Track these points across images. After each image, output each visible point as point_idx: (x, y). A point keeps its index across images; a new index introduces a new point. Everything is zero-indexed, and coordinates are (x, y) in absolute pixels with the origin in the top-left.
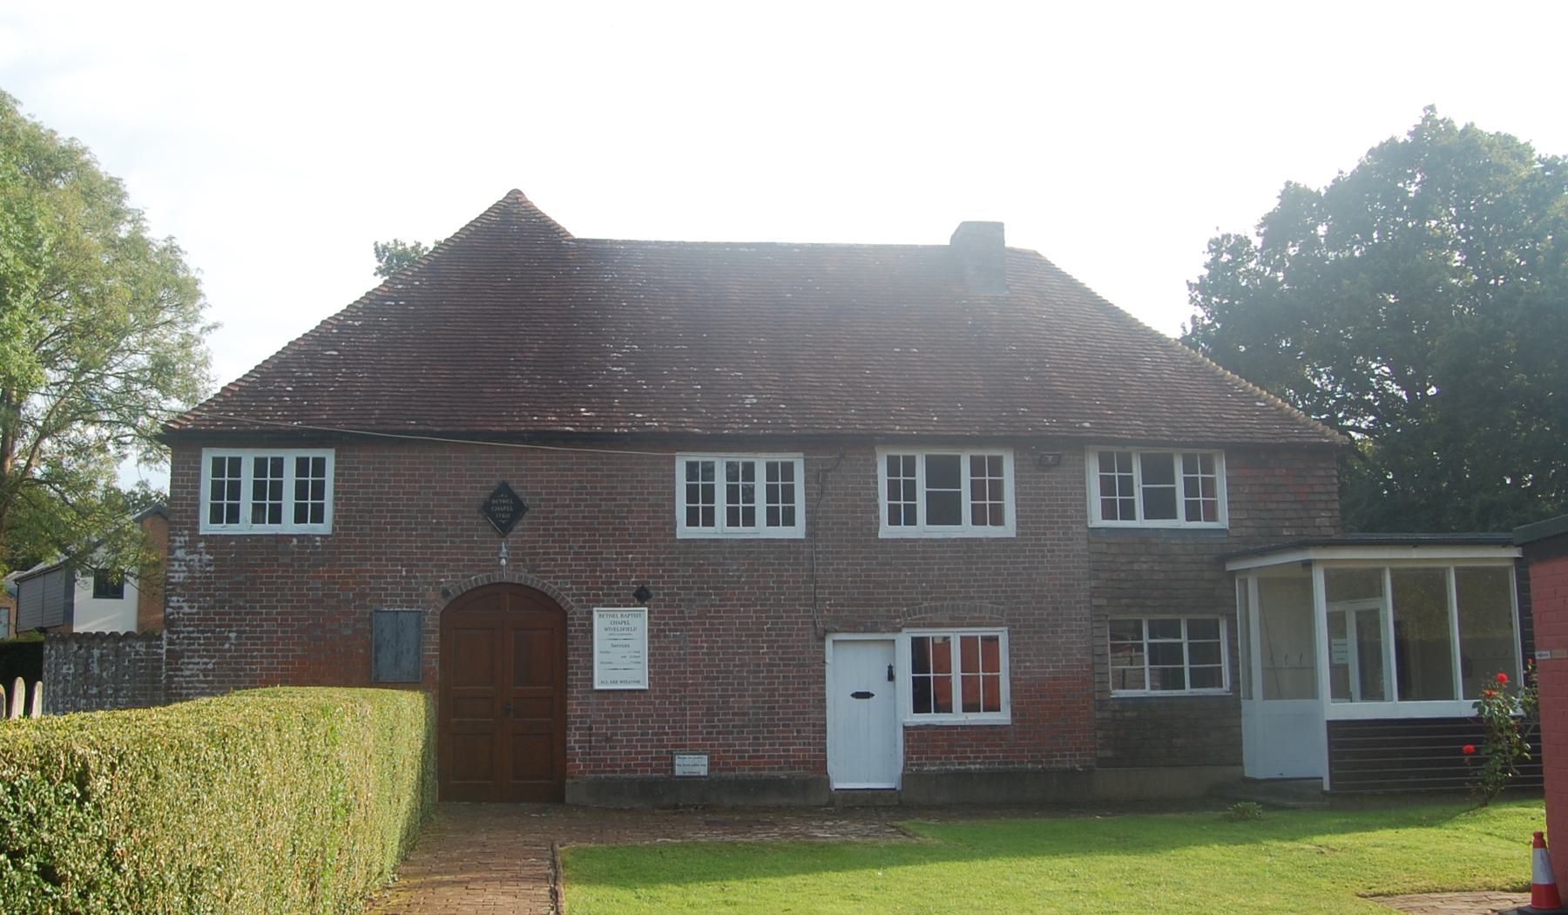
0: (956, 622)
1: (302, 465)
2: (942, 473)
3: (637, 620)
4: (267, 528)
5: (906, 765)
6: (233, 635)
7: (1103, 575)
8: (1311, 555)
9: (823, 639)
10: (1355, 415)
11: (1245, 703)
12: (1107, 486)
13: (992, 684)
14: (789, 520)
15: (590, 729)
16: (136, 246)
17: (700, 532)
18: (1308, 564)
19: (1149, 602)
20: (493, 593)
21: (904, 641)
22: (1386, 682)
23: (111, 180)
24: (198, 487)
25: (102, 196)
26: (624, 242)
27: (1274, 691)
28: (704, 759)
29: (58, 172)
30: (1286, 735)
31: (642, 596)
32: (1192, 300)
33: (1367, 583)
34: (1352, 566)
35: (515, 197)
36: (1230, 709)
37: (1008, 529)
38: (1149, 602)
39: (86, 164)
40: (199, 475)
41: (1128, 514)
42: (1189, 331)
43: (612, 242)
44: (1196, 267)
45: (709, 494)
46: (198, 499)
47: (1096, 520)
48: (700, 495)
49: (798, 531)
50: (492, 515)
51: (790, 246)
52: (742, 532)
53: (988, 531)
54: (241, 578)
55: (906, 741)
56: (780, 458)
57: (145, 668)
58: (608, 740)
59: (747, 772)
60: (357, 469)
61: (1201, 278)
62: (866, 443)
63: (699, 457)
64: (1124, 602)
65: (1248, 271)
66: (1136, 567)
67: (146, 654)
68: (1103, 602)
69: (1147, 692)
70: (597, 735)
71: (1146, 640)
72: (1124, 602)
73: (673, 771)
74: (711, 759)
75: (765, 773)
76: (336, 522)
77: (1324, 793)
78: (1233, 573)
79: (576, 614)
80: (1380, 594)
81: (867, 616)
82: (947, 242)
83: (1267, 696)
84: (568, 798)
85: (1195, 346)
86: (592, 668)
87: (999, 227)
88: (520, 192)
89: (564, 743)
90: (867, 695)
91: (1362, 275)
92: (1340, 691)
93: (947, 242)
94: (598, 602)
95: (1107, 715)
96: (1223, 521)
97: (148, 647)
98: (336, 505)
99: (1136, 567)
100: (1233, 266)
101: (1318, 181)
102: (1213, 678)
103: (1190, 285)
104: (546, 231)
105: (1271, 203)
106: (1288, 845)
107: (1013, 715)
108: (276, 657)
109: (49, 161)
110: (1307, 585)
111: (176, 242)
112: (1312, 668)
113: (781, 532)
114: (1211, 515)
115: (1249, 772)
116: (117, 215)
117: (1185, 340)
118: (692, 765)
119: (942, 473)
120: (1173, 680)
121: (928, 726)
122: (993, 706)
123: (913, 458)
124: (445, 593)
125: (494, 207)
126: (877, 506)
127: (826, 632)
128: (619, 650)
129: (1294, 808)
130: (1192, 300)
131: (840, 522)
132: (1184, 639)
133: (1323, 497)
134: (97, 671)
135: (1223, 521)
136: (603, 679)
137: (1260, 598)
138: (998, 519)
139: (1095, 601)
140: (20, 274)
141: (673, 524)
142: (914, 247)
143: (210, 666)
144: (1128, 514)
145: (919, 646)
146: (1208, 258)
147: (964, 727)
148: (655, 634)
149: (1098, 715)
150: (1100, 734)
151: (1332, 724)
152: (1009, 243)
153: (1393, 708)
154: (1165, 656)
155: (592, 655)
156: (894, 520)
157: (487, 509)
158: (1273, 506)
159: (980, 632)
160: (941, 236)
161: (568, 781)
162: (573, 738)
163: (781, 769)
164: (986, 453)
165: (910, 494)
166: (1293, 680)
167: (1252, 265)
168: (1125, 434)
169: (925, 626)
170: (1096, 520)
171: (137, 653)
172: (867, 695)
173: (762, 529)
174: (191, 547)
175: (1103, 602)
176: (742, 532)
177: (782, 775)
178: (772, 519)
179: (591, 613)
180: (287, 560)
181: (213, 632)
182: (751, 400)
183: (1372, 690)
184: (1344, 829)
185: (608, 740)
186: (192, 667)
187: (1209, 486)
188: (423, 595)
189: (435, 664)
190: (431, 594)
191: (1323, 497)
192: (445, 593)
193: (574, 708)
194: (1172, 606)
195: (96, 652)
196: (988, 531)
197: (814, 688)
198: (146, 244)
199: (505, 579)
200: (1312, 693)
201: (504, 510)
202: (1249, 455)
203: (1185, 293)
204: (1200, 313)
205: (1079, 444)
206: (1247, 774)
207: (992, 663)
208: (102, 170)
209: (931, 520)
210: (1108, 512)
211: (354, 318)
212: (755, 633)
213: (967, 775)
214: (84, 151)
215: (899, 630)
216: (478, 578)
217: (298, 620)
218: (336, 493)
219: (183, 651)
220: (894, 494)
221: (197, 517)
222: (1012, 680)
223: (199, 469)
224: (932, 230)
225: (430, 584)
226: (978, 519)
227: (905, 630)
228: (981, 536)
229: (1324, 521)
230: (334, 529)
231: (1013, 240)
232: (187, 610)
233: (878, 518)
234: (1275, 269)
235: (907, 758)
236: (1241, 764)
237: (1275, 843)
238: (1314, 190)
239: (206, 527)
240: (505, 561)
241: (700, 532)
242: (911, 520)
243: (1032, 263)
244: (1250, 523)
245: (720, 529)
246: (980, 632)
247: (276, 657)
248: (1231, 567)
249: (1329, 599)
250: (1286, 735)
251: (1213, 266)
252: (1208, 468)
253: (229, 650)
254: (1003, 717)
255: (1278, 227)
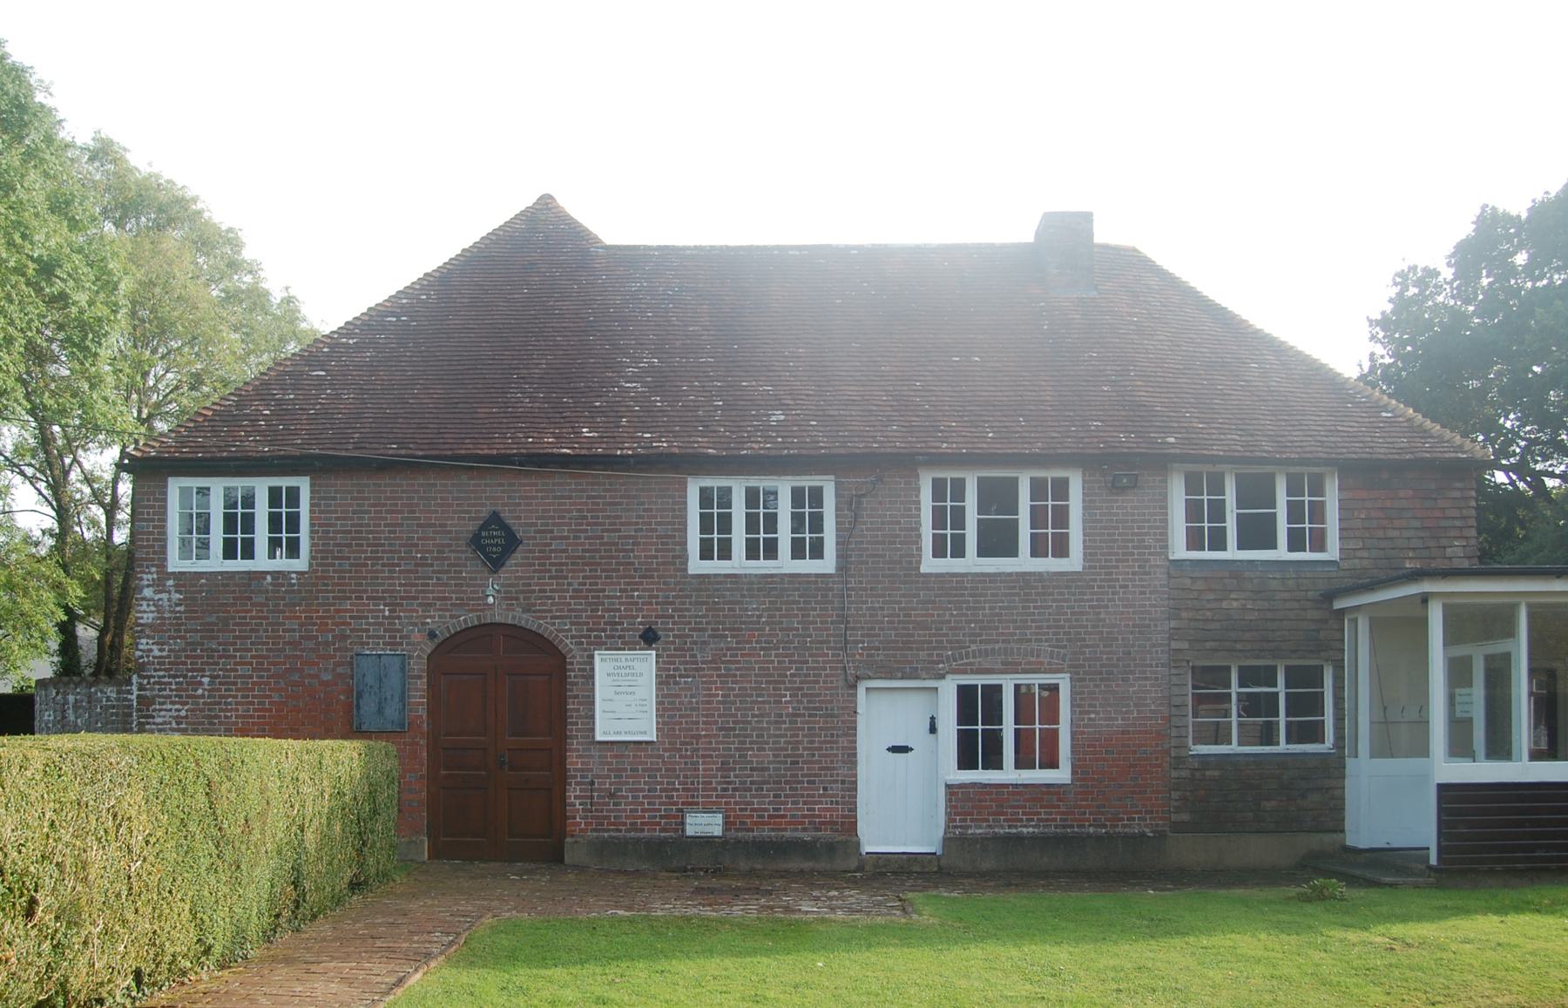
0: (1010, 668)
1: (274, 495)
2: (998, 497)
3: (645, 664)
4: (239, 565)
5: (947, 827)
6: (206, 680)
7: (1184, 615)
8: (1427, 587)
9: (855, 687)
10: (1545, 458)
11: (1349, 762)
12: (1193, 511)
13: (1051, 739)
14: (817, 552)
15: (592, 783)
16: (257, 298)
17: (715, 567)
18: (1425, 599)
19: (1239, 646)
20: (483, 635)
21: (948, 691)
22: (1515, 737)
23: (230, 230)
24: (165, 520)
25: (216, 245)
26: (659, 248)
27: (1385, 748)
28: (719, 818)
29: (170, 220)
30: (1391, 802)
31: (649, 638)
32: (1373, 338)
33: (1496, 621)
34: (1478, 600)
35: (546, 202)
36: (1332, 769)
37: (1074, 561)
38: (1239, 646)
39: (199, 213)
40: (165, 507)
41: (1218, 542)
42: (1366, 370)
43: (647, 248)
44: (1380, 302)
45: (726, 523)
46: (165, 533)
47: (1179, 550)
48: (716, 522)
49: (827, 564)
50: (482, 548)
51: (847, 248)
52: (763, 566)
53: (1050, 564)
54: (213, 619)
55: (948, 800)
56: (807, 482)
57: (117, 715)
58: (612, 796)
59: (766, 833)
60: (334, 499)
61: (1383, 313)
62: (906, 463)
63: (714, 482)
64: (1209, 645)
65: (1436, 305)
66: (1225, 604)
67: (118, 700)
68: (1186, 645)
69: (1234, 748)
70: (600, 790)
71: (1235, 689)
72: (1209, 645)
73: (683, 830)
74: (726, 817)
75: (787, 834)
76: (312, 558)
77: (1431, 868)
78: (1342, 611)
79: (576, 657)
80: (1511, 633)
81: (904, 662)
82: (1032, 240)
83: (1376, 753)
84: (567, 860)
85: (1374, 385)
86: (593, 717)
87: (1087, 217)
88: (550, 197)
89: (563, 798)
90: (904, 749)
91: (1558, 303)
92: (1460, 747)
93: (1032, 240)
94: (600, 645)
95: (1185, 773)
96: (1332, 552)
97: (119, 692)
98: (312, 538)
99: (1225, 604)
100: (1419, 300)
101: (1519, 206)
102: (1313, 733)
103: (1370, 321)
104: (576, 235)
105: (1465, 229)
106: (1352, 936)
107: (1074, 772)
108: (252, 703)
109: (160, 210)
110: (1423, 622)
111: (292, 292)
112: (1424, 724)
113: (808, 566)
114: (1319, 543)
115: (1351, 840)
116: (234, 265)
117: (1362, 378)
118: (704, 824)
119: (998, 497)
120: (1268, 736)
121: (974, 785)
122: (1051, 762)
123: (963, 481)
124: (432, 635)
125: (522, 213)
126: (919, 536)
127: (858, 678)
128: (623, 698)
129: (1391, 885)
130: (1373, 338)
131: (877, 557)
132: (1281, 688)
133: (1458, 523)
134: (72, 718)
135: (1332, 552)
136: (604, 731)
137: (1372, 638)
138: (1061, 550)
139: (1174, 645)
140: (100, 320)
141: (684, 558)
142: (830, 246)
143: (183, 713)
144: (1218, 542)
145: (965, 694)
146: (1394, 291)
147: (1016, 786)
148: (663, 681)
149: (1174, 774)
150: (1175, 795)
151: (1443, 789)
152: (1099, 238)
153: (1522, 769)
154: (1257, 706)
155: (593, 703)
156: (939, 552)
157: (476, 542)
158: (1396, 533)
159: (1036, 680)
160: (1019, 230)
161: (568, 840)
162: (574, 793)
163: (805, 830)
164: (1050, 474)
165: (959, 522)
166: (1401, 735)
167: (1440, 299)
168: (1217, 451)
169: (972, 672)
170: (1179, 550)
171: (108, 699)
172: (904, 749)
173: (785, 563)
174: (159, 585)
175: (1186, 645)
176: (763, 566)
177: (806, 836)
178: (798, 551)
179: (592, 657)
180: (260, 599)
181: (185, 677)
182: (778, 416)
183: (1499, 748)
184: (1441, 913)
185: (612, 796)
186: (166, 712)
187: (1318, 512)
188: (406, 637)
189: (422, 712)
190: (417, 636)
191: (1458, 523)
192: (432, 635)
193: (574, 761)
194: (1277, 653)
195: (71, 698)
196: (1050, 564)
197: (843, 742)
198: (267, 293)
199: (498, 619)
200: (1423, 751)
201: (495, 543)
202: (1363, 474)
203: (1365, 330)
204: (1379, 350)
205: (1160, 463)
206: (1348, 843)
207: (1051, 714)
208: (216, 220)
209: (982, 552)
210: (1194, 541)
211: (349, 335)
212: (778, 676)
213: (1019, 838)
214: (195, 200)
215: (943, 677)
216: (468, 619)
217: (275, 664)
218: (312, 525)
219: (154, 697)
220: (939, 522)
221: (165, 553)
222: (1073, 734)
223: (165, 500)
224: (1008, 223)
225: (415, 624)
226: (1037, 550)
227: (949, 677)
228: (1041, 569)
229: (1458, 551)
230: (311, 565)
231: (1105, 234)
232: (157, 653)
233: (920, 549)
234: (1467, 302)
235: (950, 819)
236: (1343, 831)
237: (1338, 933)
238: (1514, 213)
239: (175, 563)
240: (494, 598)
241: (715, 567)
242: (959, 552)
243: (1130, 267)
244: (1365, 554)
245: (739, 564)
246: (1036, 680)
247: (252, 703)
248: (1339, 604)
249: (1449, 641)
250: (1391, 802)
251: (1400, 302)
252: (1317, 489)
253: (203, 696)
254: (1062, 775)
255: (1469, 256)
